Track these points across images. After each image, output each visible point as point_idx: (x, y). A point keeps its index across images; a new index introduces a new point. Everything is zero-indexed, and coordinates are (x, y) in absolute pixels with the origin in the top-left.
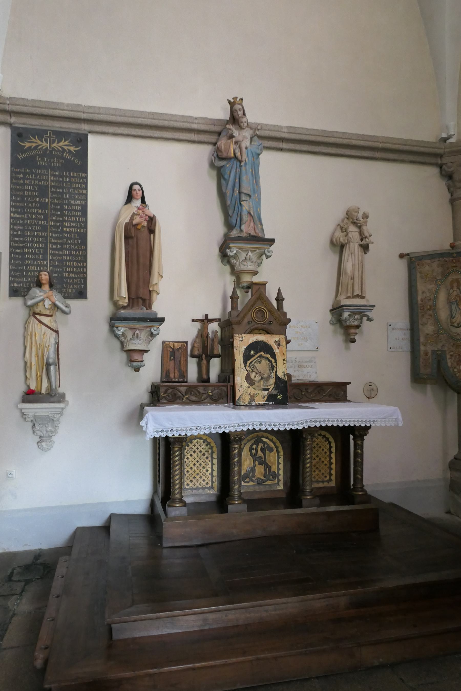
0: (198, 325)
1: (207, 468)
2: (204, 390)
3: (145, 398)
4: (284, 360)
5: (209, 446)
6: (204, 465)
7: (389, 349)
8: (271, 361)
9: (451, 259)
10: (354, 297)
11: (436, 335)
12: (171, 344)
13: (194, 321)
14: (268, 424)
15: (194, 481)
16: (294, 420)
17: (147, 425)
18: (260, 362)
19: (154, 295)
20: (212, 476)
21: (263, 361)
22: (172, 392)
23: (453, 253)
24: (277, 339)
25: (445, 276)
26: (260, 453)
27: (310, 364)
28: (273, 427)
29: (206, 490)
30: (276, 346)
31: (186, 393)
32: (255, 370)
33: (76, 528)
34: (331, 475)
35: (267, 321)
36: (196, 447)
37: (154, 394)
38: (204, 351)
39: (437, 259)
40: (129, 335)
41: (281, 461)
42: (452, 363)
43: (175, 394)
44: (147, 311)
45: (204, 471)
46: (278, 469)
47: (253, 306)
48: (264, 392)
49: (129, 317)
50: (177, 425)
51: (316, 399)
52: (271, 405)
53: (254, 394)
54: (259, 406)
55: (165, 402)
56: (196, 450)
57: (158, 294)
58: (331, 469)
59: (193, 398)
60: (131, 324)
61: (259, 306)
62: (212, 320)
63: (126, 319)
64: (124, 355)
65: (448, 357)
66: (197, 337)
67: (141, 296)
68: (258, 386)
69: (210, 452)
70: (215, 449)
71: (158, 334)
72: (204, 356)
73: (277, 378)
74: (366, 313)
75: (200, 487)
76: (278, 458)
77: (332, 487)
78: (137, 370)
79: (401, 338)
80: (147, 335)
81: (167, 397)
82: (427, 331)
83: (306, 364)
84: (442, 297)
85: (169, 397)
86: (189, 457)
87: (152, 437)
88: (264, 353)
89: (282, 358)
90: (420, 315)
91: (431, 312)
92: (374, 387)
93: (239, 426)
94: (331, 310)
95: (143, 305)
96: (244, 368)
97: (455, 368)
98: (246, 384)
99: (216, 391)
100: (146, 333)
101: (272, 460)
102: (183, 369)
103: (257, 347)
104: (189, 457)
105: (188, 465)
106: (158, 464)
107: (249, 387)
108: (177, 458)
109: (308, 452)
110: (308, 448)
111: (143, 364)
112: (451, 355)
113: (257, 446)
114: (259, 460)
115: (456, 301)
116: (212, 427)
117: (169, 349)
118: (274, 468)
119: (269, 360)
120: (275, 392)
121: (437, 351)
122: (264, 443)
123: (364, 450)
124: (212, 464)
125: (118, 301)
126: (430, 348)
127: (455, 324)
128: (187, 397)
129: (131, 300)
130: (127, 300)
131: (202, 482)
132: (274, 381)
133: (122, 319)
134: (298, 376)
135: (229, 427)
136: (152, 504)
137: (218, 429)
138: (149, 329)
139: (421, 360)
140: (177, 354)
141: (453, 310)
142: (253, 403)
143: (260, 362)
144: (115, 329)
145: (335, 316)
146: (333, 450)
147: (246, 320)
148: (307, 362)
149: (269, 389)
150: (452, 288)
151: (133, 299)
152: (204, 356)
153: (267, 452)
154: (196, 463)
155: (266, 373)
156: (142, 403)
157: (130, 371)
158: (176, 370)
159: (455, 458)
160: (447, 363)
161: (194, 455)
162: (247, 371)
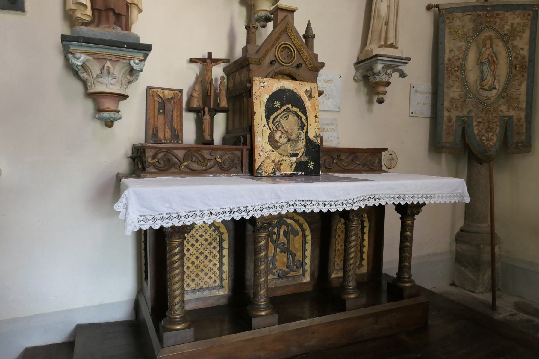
0: (196, 69)
1: (215, 261)
2: (211, 155)
3: (124, 166)
4: (316, 116)
5: (217, 232)
6: (210, 257)
7: (411, 115)
8: (301, 118)
9: (485, 12)
10: (386, 45)
11: (462, 99)
12: (160, 92)
13: (192, 61)
14: (315, 203)
15: (197, 279)
16: (348, 197)
17: (127, 209)
18: (287, 118)
19: (134, 11)
20: (222, 272)
21: (291, 117)
22: (164, 156)
23: (487, 6)
24: (308, 89)
25: (477, 32)
26: (283, 239)
27: (332, 127)
28: (321, 208)
29: (214, 290)
30: (306, 97)
31: (185, 158)
32: (280, 129)
33: (23, 349)
34: (362, 259)
35: (295, 62)
36: (199, 234)
37: (136, 160)
38: (205, 104)
39: (470, 13)
40: (95, 68)
41: (308, 246)
42: (479, 131)
43: (169, 160)
44: (123, 31)
45: (211, 265)
46: (304, 256)
47: (277, 40)
48: (291, 158)
49: (94, 37)
50: (179, 208)
51: (349, 168)
52: (300, 175)
53: (279, 161)
54: (285, 177)
55: (152, 171)
56: (199, 238)
57: (140, 11)
58: (362, 252)
59: (195, 166)
60: (97, 50)
61: (284, 41)
62: (216, 61)
63: (88, 41)
64: (89, 105)
65: (475, 123)
66: (195, 83)
67: (112, 7)
68: (284, 151)
69: (218, 239)
70: (226, 236)
71: (141, 71)
72: (206, 109)
73: (308, 140)
74: (400, 67)
75: (205, 287)
76: (305, 243)
77: (362, 275)
78: (109, 124)
79: (422, 102)
80: (123, 71)
81: (157, 164)
82: (452, 95)
83: (327, 127)
84: (472, 56)
85: (160, 164)
86: (190, 248)
87: (137, 229)
88: (292, 106)
89: (314, 115)
90: (446, 77)
91: (458, 74)
92: (394, 156)
93: (274, 207)
94: (356, 64)
95: (116, 25)
96: (266, 125)
97: (483, 135)
98: (269, 148)
99: (227, 156)
100: (123, 68)
101: (297, 246)
102: (177, 127)
103: (280, 98)
104: (190, 248)
105: (189, 259)
106: (143, 255)
107: (273, 151)
108: (177, 257)
109: (353, 238)
110: (353, 233)
111: (119, 116)
112: (479, 122)
113: (279, 228)
114: (281, 247)
115: (489, 61)
116: (236, 210)
117: (156, 98)
118: (299, 256)
119: (298, 116)
120: (305, 159)
121: (463, 117)
122: (288, 225)
123: (414, 232)
124: (222, 256)
125: (74, 10)
126: (454, 114)
127: (486, 87)
128: (185, 164)
129: (96, 13)
130: (89, 12)
131: (208, 280)
132: (305, 144)
133: (81, 40)
134: (332, 141)
135: (261, 209)
136: (137, 307)
137: (244, 213)
138: (127, 61)
139: (444, 127)
140: (168, 106)
141: (485, 72)
142: (278, 174)
143: (287, 118)
144: (70, 56)
145: (360, 71)
146: (366, 230)
147: (268, 60)
148: (328, 124)
149: (298, 154)
150: (485, 46)
151: (99, 11)
152: (206, 109)
153: (291, 236)
154: (199, 256)
155: (295, 132)
156: (118, 173)
157: (98, 125)
158: (167, 128)
159: (461, 230)
160: (473, 131)
161: (197, 245)
162: (270, 129)
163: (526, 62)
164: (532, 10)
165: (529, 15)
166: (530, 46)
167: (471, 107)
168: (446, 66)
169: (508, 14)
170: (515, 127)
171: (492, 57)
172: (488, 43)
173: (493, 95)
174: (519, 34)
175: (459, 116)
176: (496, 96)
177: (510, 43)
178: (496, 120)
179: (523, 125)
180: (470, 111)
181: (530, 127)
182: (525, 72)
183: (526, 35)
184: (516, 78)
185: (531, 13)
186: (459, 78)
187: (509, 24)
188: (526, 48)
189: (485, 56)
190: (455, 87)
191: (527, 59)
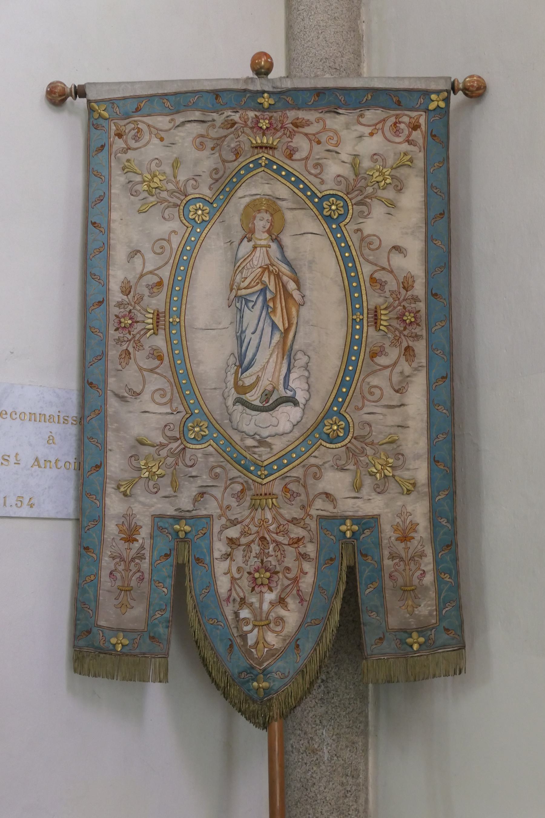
9: (251, 114)
11: (174, 445)
25: (226, 186)
39: (197, 115)
65: (220, 548)
90: (113, 353)
91: (160, 342)
112: (232, 542)
121: (177, 519)
126: (147, 506)
127: (254, 397)
141: (248, 333)
150: (249, 234)
163: (416, 299)
164: (427, 110)
165: (416, 127)
166: (429, 239)
167: (205, 479)
168: (114, 310)
169: (335, 122)
170: (387, 562)
171: (278, 276)
172: (261, 222)
173: (284, 426)
174: (380, 193)
175: (161, 517)
176: (296, 433)
177: (352, 227)
178: (297, 532)
179: (422, 555)
180: (202, 494)
181: (456, 560)
182: (417, 337)
183: (413, 198)
184: (382, 360)
185: (422, 121)
186: (160, 358)
187: (344, 157)
188: (415, 246)
189: (251, 274)
190: (146, 396)
191: (419, 289)
